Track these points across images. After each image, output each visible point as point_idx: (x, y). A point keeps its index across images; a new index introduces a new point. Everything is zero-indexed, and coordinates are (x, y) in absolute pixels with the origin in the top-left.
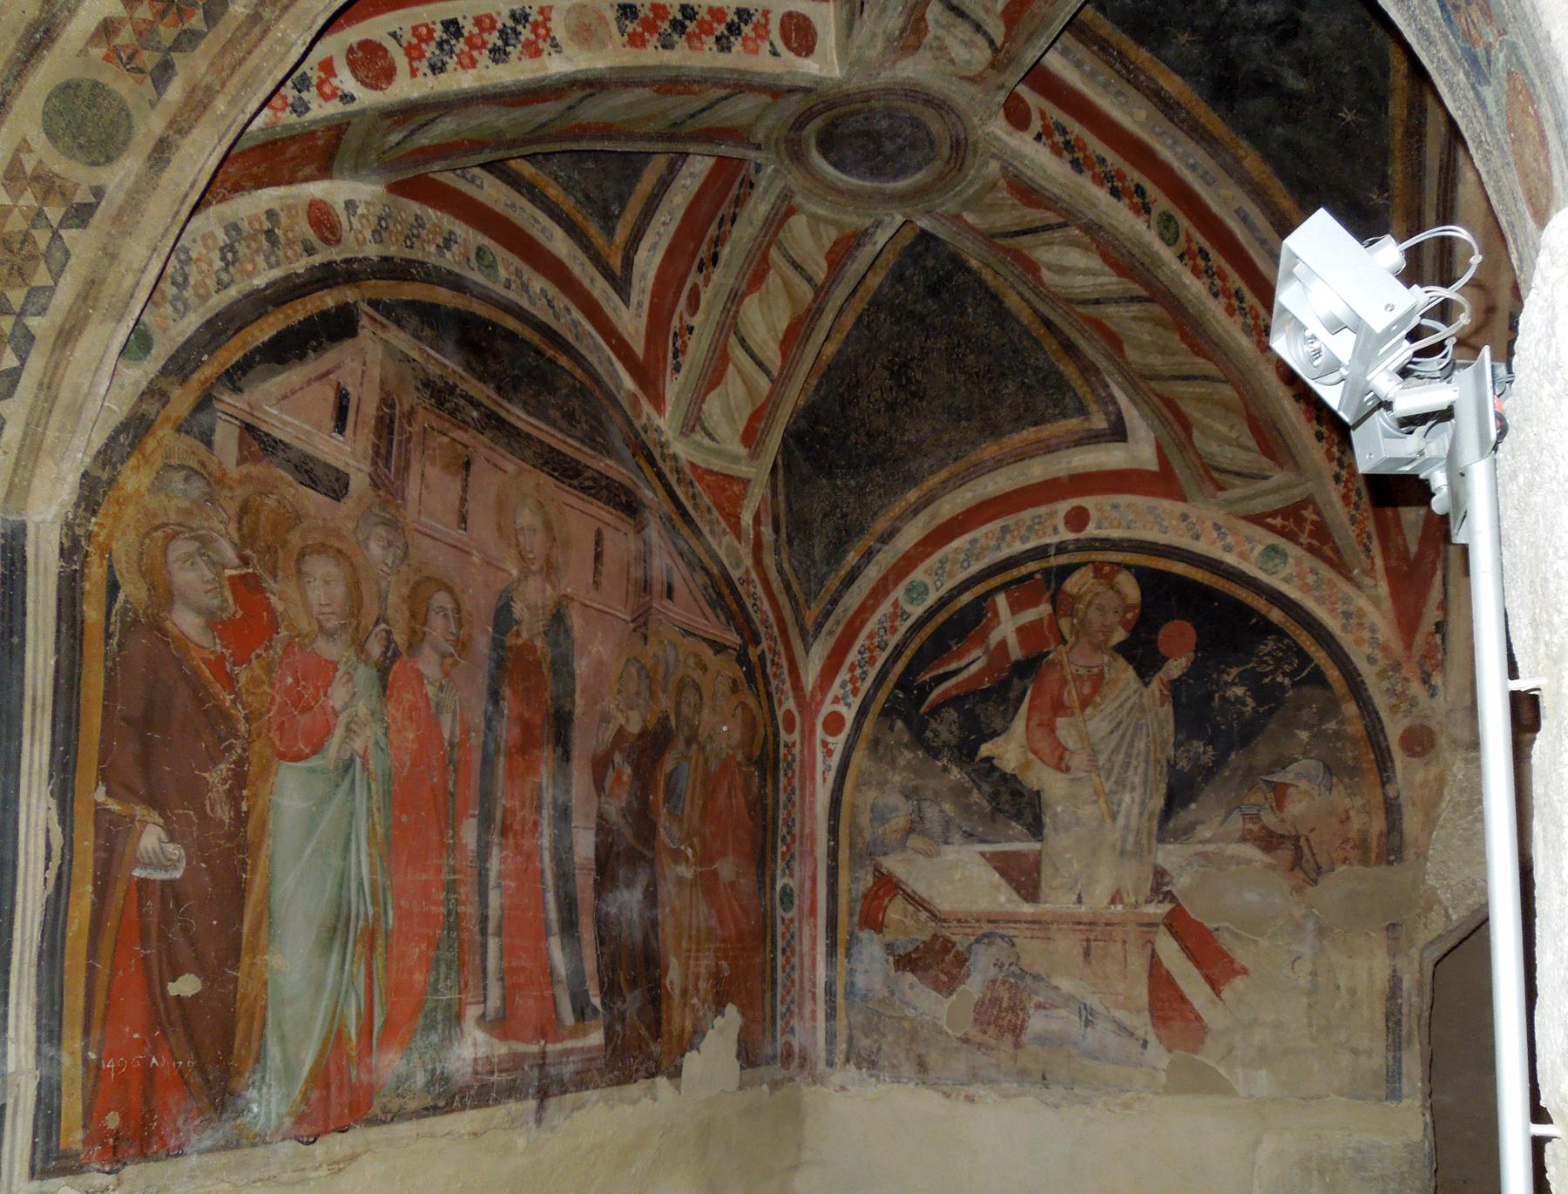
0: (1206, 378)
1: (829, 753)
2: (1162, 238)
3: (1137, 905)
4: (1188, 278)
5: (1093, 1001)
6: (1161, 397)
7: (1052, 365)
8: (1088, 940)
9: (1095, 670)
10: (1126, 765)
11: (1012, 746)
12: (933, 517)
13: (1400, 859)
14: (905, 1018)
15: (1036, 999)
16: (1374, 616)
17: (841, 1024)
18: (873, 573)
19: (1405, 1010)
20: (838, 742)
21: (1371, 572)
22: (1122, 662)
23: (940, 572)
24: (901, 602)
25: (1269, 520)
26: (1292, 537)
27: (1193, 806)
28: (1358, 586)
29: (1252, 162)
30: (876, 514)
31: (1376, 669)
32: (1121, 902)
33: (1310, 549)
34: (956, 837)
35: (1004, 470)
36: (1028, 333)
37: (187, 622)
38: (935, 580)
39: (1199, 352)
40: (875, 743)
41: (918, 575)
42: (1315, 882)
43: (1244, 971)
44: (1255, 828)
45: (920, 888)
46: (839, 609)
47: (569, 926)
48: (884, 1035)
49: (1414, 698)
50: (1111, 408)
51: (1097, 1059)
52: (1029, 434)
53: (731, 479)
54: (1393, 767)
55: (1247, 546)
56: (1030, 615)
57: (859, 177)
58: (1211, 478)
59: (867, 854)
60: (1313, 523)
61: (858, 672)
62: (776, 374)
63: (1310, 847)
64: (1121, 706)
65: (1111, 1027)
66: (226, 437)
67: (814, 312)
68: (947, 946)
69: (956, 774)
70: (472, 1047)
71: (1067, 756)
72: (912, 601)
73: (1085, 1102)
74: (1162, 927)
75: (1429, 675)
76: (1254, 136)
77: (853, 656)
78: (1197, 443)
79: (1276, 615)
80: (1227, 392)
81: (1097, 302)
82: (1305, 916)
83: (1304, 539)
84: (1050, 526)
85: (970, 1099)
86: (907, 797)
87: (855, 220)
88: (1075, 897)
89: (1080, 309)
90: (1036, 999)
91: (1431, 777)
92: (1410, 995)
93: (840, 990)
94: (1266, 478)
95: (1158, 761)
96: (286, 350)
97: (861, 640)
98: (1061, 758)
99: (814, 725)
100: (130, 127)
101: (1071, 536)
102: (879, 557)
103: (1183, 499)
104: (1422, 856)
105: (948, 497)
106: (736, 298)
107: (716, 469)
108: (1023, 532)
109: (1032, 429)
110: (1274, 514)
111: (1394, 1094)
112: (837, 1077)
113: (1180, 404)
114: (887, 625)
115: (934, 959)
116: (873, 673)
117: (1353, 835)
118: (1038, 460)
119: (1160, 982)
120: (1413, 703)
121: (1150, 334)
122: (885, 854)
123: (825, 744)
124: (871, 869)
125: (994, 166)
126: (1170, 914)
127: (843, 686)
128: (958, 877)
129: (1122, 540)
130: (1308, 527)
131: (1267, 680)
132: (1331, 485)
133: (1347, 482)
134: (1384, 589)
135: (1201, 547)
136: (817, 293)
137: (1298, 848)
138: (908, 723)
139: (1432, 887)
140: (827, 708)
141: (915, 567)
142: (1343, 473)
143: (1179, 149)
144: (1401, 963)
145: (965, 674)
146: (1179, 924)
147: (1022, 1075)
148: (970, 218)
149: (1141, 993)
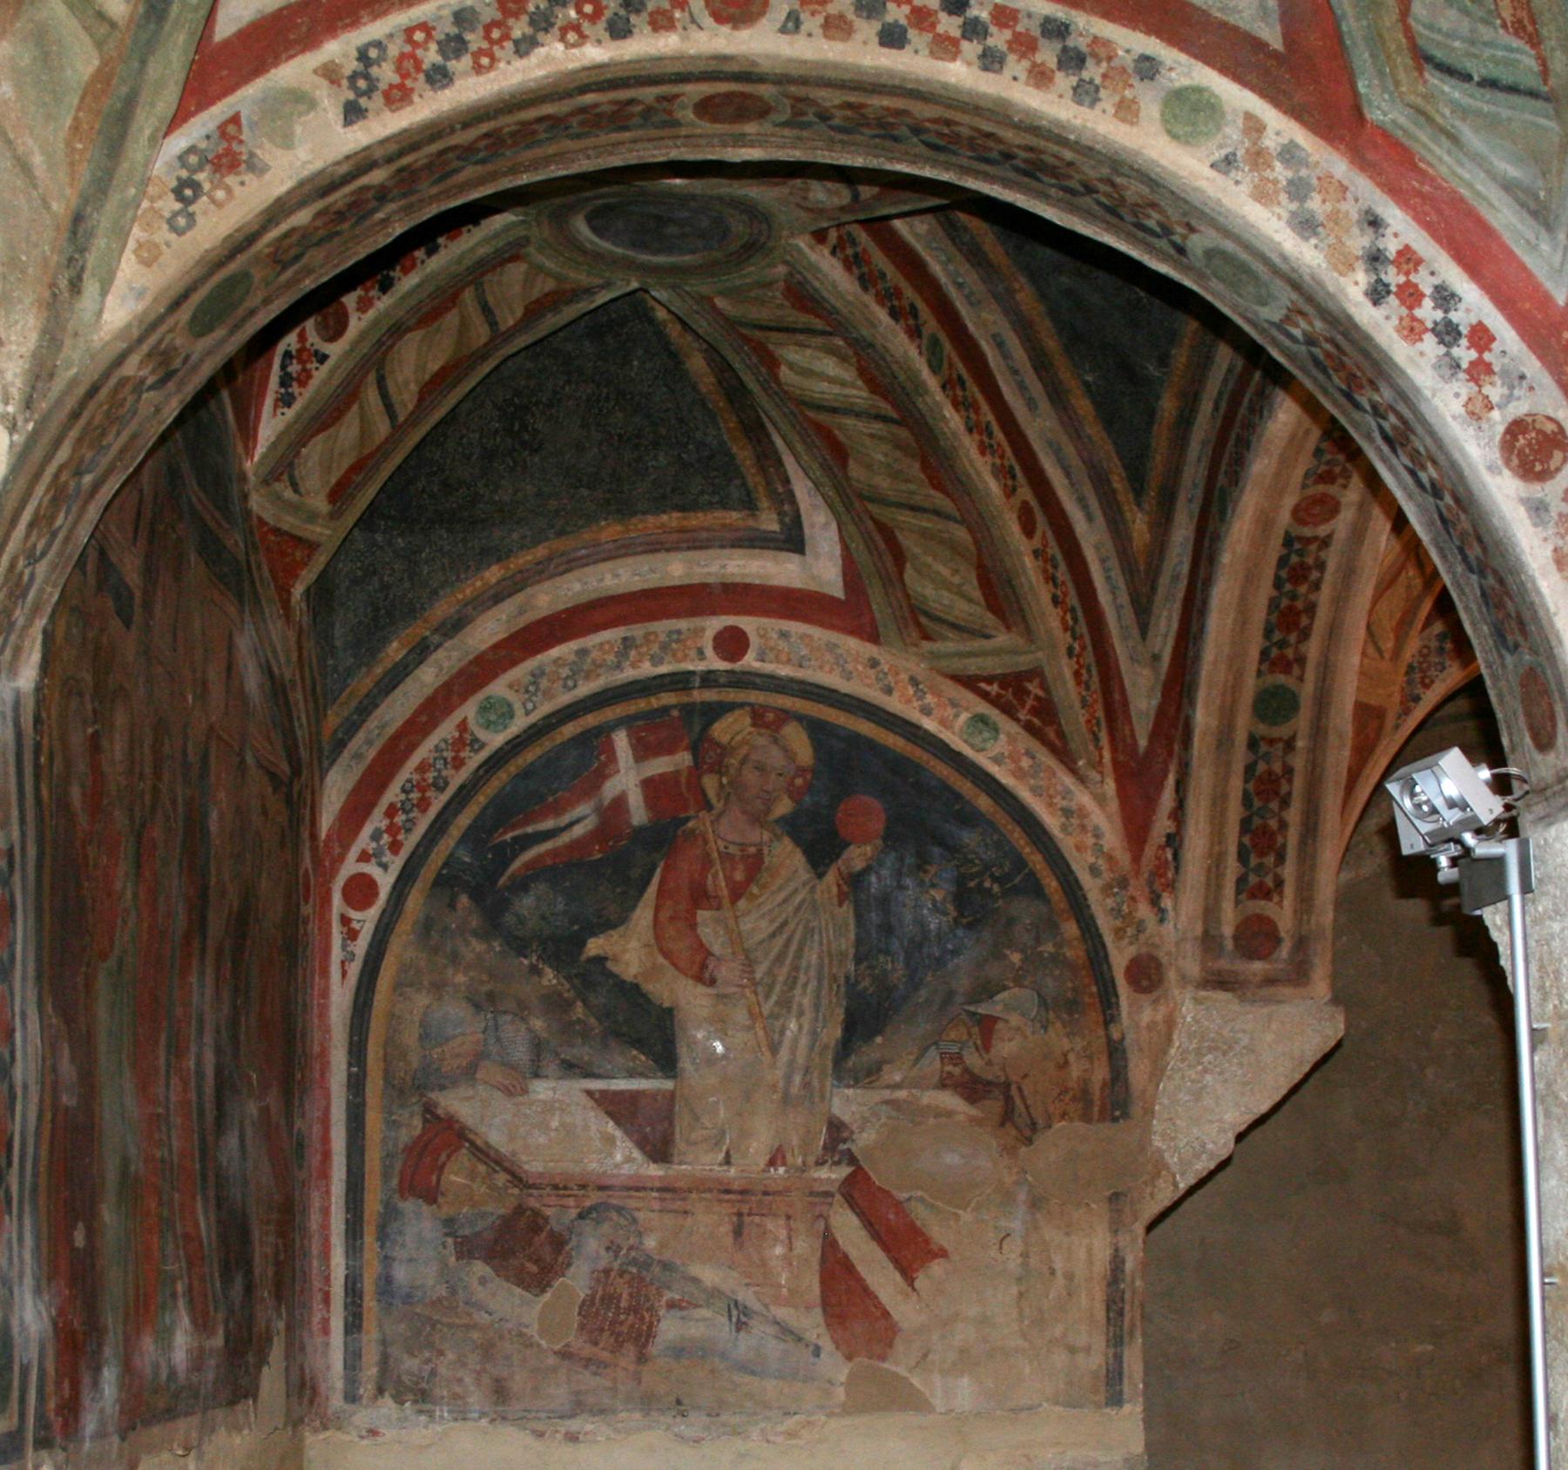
0: (937, 513)
1: (352, 935)
2: (930, 366)
3: (804, 1168)
4: (949, 412)
5: (747, 1296)
6: (876, 522)
7: (722, 443)
8: (740, 1214)
9: (752, 850)
10: (792, 982)
11: (634, 944)
12: (521, 612)
13: (1126, 1115)
14: (475, 1326)
15: (668, 1295)
16: (1098, 818)
17: (370, 1337)
18: (428, 677)
19: (1127, 1296)
20: (367, 920)
21: (1097, 765)
22: (787, 844)
23: (531, 688)
24: (472, 725)
25: (983, 685)
26: (1008, 711)
27: (879, 1040)
28: (1082, 780)
29: (1026, 296)
30: (435, 592)
31: (1100, 882)
32: (784, 1164)
33: (1029, 728)
34: (551, 1068)
35: (630, 560)
36: (703, 403)
38: (519, 700)
39: (938, 486)
40: (426, 927)
41: (498, 688)
42: (1029, 1141)
43: (943, 1254)
44: (957, 1071)
45: (496, 1138)
46: (372, 723)
48: (441, 1353)
49: (1141, 922)
50: (786, 507)
51: (753, 1373)
52: (671, 519)
53: (298, 541)
54: (1117, 1004)
55: (950, 711)
56: (660, 766)
57: (614, 243)
58: (918, 624)
59: (416, 1086)
60: (1037, 698)
61: (400, 819)
62: (401, 419)
63: (1023, 1097)
64: (785, 901)
65: (771, 1330)
67: (482, 355)
68: (537, 1223)
69: (550, 977)
71: (711, 964)
72: (488, 725)
73: (736, 1432)
74: (838, 1197)
75: (1159, 897)
76: (1034, 277)
77: (393, 794)
78: (907, 577)
79: (984, 803)
80: (961, 534)
81: (835, 410)
82: (1017, 1183)
83: (1023, 715)
84: (695, 646)
85: (573, 1438)
86: (478, 1007)
87: (579, 277)
88: (721, 1156)
89: (811, 414)
90: (668, 1295)
91: (1159, 1017)
92: (1133, 1281)
93: (368, 1285)
94: (988, 637)
95: (834, 978)
97: (407, 772)
98: (703, 966)
99: (329, 892)
101: (722, 665)
102: (440, 654)
103: (874, 638)
104: (1149, 1112)
105: (547, 585)
106: (397, 331)
107: (286, 527)
108: (655, 649)
109: (675, 515)
110: (989, 680)
111: (1116, 1400)
112: (363, 1416)
113: (898, 533)
114: (449, 755)
115: (523, 1240)
116: (423, 823)
117: (1072, 1084)
118: (680, 555)
119: (837, 1272)
120: (1140, 927)
121: (886, 455)
122: (442, 1088)
123: (345, 920)
124: (417, 1109)
125: (781, 270)
126: (849, 1181)
127: (376, 836)
128: (555, 1125)
129: (792, 680)
130: (1030, 703)
131: (972, 884)
132: (1064, 660)
133: (1078, 656)
134: (1110, 787)
135: (894, 704)
136: (491, 340)
137: (1008, 1099)
138: (477, 895)
139: (1159, 1150)
140: (350, 867)
141: (495, 676)
142: (1076, 646)
143: (951, 267)
144: (1124, 1240)
145: (565, 839)
146: (859, 1191)
147: (647, 1403)
148: (720, 303)
149: (812, 1284)
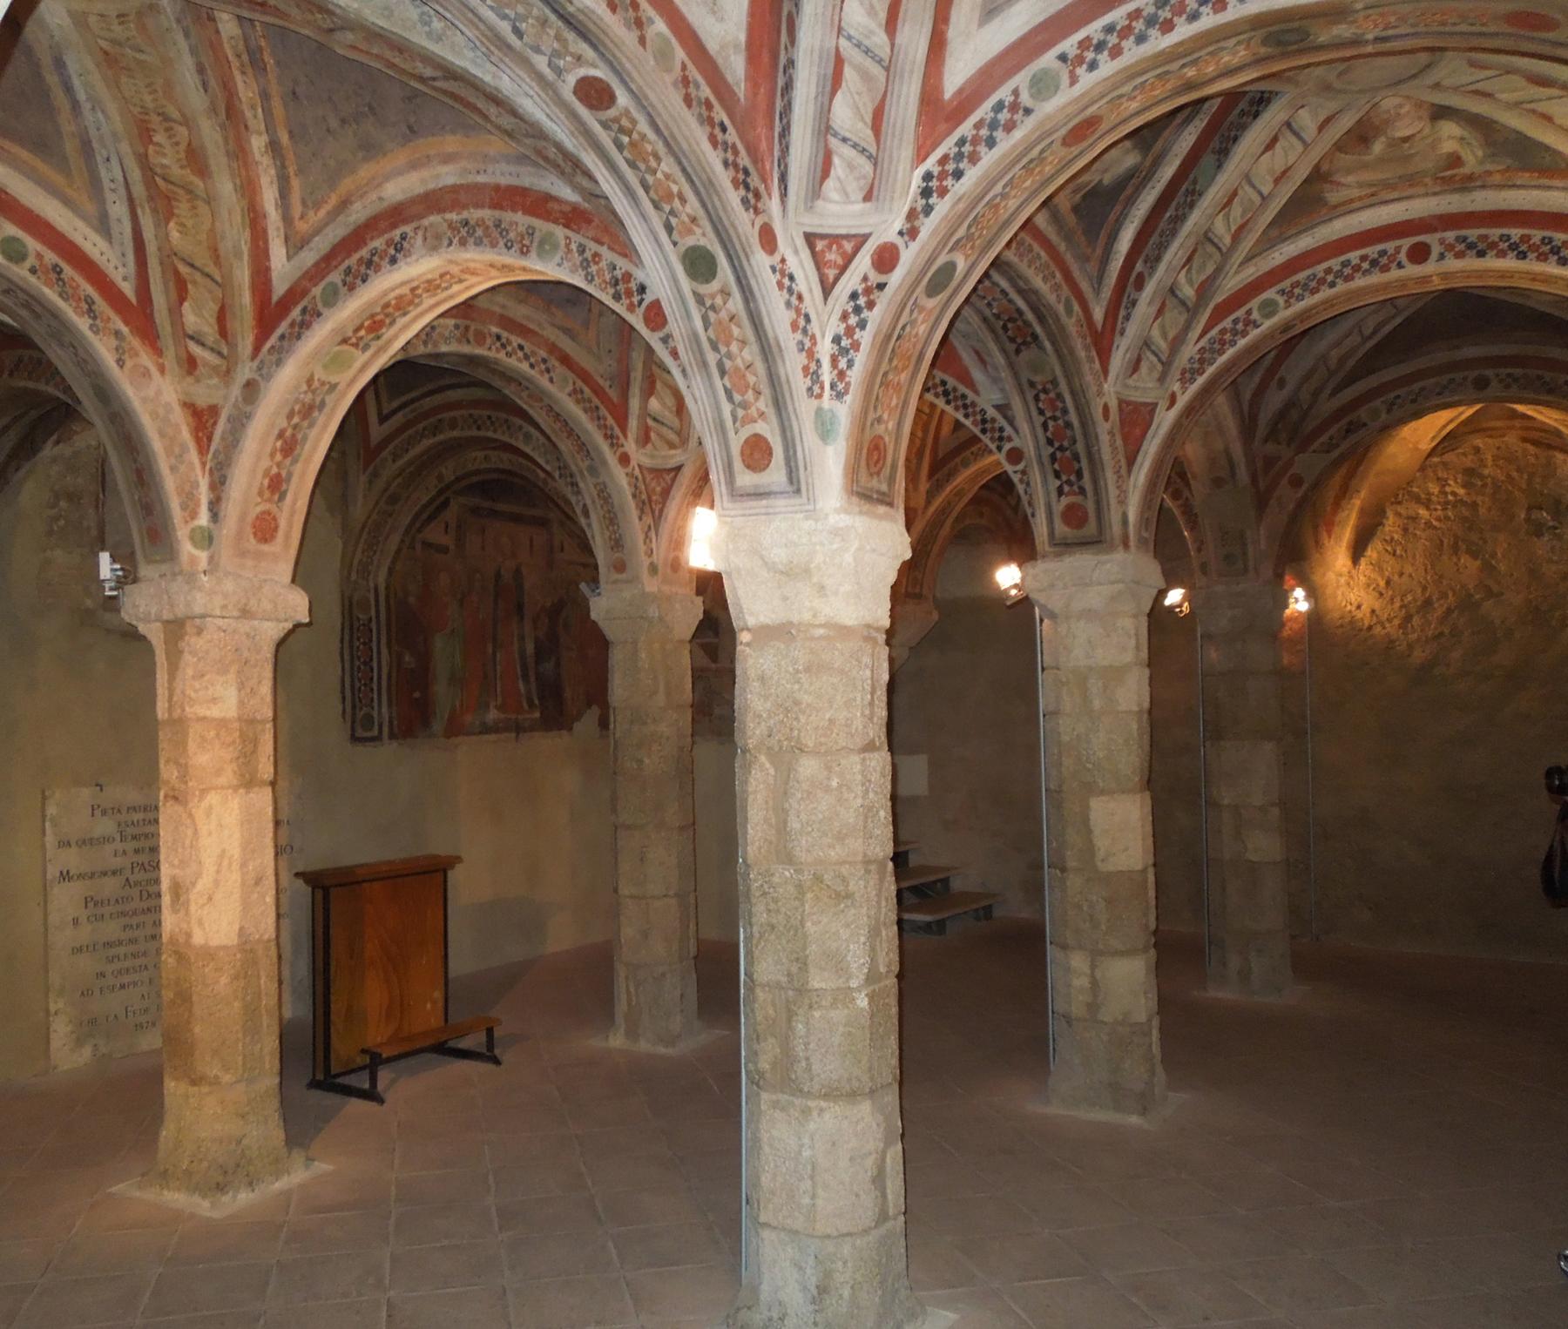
37: (412, 600)
47: (525, 677)
66: (418, 546)
70: (493, 715)
96: (430, 519)
100: (196, 832)
